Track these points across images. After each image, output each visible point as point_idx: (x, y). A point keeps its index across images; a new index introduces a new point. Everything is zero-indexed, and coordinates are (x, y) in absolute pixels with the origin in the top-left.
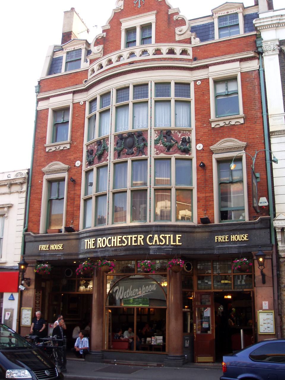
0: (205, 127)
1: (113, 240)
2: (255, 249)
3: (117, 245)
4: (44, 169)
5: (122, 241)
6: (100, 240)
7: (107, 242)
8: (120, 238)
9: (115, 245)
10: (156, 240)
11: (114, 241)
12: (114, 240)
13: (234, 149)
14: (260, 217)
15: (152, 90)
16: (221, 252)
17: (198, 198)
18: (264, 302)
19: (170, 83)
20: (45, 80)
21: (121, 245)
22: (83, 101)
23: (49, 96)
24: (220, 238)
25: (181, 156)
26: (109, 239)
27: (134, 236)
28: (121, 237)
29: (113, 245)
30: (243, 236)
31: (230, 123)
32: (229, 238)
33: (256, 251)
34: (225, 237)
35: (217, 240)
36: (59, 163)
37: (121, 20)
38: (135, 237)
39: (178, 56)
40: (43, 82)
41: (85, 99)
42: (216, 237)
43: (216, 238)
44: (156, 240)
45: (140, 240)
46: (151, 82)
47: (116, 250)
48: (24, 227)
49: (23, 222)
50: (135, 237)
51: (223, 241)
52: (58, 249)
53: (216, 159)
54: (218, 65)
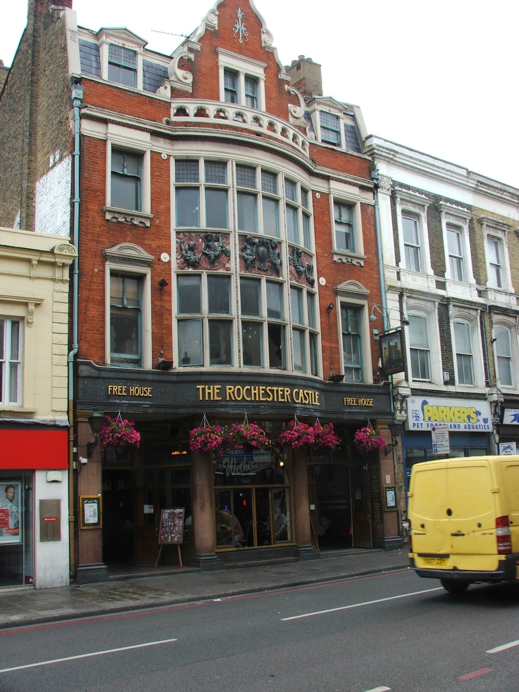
0: (326, 257)
1: (253, 392)
2: (379, 416)
3: (214, 398)
4: (114, 251)
5: (266, 394)
6: (230, 389)
7: (243, 392)
8: (263, 390)
9: (257, 399)
10: (302, 397)
11: (255, 394)
12: (209, 391)
13: (130, 261)
14: (384, 381)
15: (231, 173)
16: (350, 417)
17: (323, 347)
18: (387, 476)
19: (197, 161)
20: (91, 82)
21: (265, 399)
22: (167, 153)
23: (110, 120)
24: (349, 400)
25: (193, 271)
26: (247, 389)
27: (280, 389)
28: (264, 388)
29: (253, 399)
30: (146, 389)
31: (133, 221)
32: (128, 391)
33: (91, 410)
34: (122, 388)
35: (112, 391)
36: (140, 250)
37: (220, 49)
38: (281, 390)
39: (192, 119)
40: (87, 83)
41: (170, 152)
42: (110, 386)
43: (110, 389)
44: (302, 397)
45: (229, 393)
46: (232, 161)
47: (272, 407)
48: (70, 349)
49: (65, 339)
50: (281, 390)
51: (119, 394)
52: (144, 396)
53: (111, 270)
54: (134, 130)
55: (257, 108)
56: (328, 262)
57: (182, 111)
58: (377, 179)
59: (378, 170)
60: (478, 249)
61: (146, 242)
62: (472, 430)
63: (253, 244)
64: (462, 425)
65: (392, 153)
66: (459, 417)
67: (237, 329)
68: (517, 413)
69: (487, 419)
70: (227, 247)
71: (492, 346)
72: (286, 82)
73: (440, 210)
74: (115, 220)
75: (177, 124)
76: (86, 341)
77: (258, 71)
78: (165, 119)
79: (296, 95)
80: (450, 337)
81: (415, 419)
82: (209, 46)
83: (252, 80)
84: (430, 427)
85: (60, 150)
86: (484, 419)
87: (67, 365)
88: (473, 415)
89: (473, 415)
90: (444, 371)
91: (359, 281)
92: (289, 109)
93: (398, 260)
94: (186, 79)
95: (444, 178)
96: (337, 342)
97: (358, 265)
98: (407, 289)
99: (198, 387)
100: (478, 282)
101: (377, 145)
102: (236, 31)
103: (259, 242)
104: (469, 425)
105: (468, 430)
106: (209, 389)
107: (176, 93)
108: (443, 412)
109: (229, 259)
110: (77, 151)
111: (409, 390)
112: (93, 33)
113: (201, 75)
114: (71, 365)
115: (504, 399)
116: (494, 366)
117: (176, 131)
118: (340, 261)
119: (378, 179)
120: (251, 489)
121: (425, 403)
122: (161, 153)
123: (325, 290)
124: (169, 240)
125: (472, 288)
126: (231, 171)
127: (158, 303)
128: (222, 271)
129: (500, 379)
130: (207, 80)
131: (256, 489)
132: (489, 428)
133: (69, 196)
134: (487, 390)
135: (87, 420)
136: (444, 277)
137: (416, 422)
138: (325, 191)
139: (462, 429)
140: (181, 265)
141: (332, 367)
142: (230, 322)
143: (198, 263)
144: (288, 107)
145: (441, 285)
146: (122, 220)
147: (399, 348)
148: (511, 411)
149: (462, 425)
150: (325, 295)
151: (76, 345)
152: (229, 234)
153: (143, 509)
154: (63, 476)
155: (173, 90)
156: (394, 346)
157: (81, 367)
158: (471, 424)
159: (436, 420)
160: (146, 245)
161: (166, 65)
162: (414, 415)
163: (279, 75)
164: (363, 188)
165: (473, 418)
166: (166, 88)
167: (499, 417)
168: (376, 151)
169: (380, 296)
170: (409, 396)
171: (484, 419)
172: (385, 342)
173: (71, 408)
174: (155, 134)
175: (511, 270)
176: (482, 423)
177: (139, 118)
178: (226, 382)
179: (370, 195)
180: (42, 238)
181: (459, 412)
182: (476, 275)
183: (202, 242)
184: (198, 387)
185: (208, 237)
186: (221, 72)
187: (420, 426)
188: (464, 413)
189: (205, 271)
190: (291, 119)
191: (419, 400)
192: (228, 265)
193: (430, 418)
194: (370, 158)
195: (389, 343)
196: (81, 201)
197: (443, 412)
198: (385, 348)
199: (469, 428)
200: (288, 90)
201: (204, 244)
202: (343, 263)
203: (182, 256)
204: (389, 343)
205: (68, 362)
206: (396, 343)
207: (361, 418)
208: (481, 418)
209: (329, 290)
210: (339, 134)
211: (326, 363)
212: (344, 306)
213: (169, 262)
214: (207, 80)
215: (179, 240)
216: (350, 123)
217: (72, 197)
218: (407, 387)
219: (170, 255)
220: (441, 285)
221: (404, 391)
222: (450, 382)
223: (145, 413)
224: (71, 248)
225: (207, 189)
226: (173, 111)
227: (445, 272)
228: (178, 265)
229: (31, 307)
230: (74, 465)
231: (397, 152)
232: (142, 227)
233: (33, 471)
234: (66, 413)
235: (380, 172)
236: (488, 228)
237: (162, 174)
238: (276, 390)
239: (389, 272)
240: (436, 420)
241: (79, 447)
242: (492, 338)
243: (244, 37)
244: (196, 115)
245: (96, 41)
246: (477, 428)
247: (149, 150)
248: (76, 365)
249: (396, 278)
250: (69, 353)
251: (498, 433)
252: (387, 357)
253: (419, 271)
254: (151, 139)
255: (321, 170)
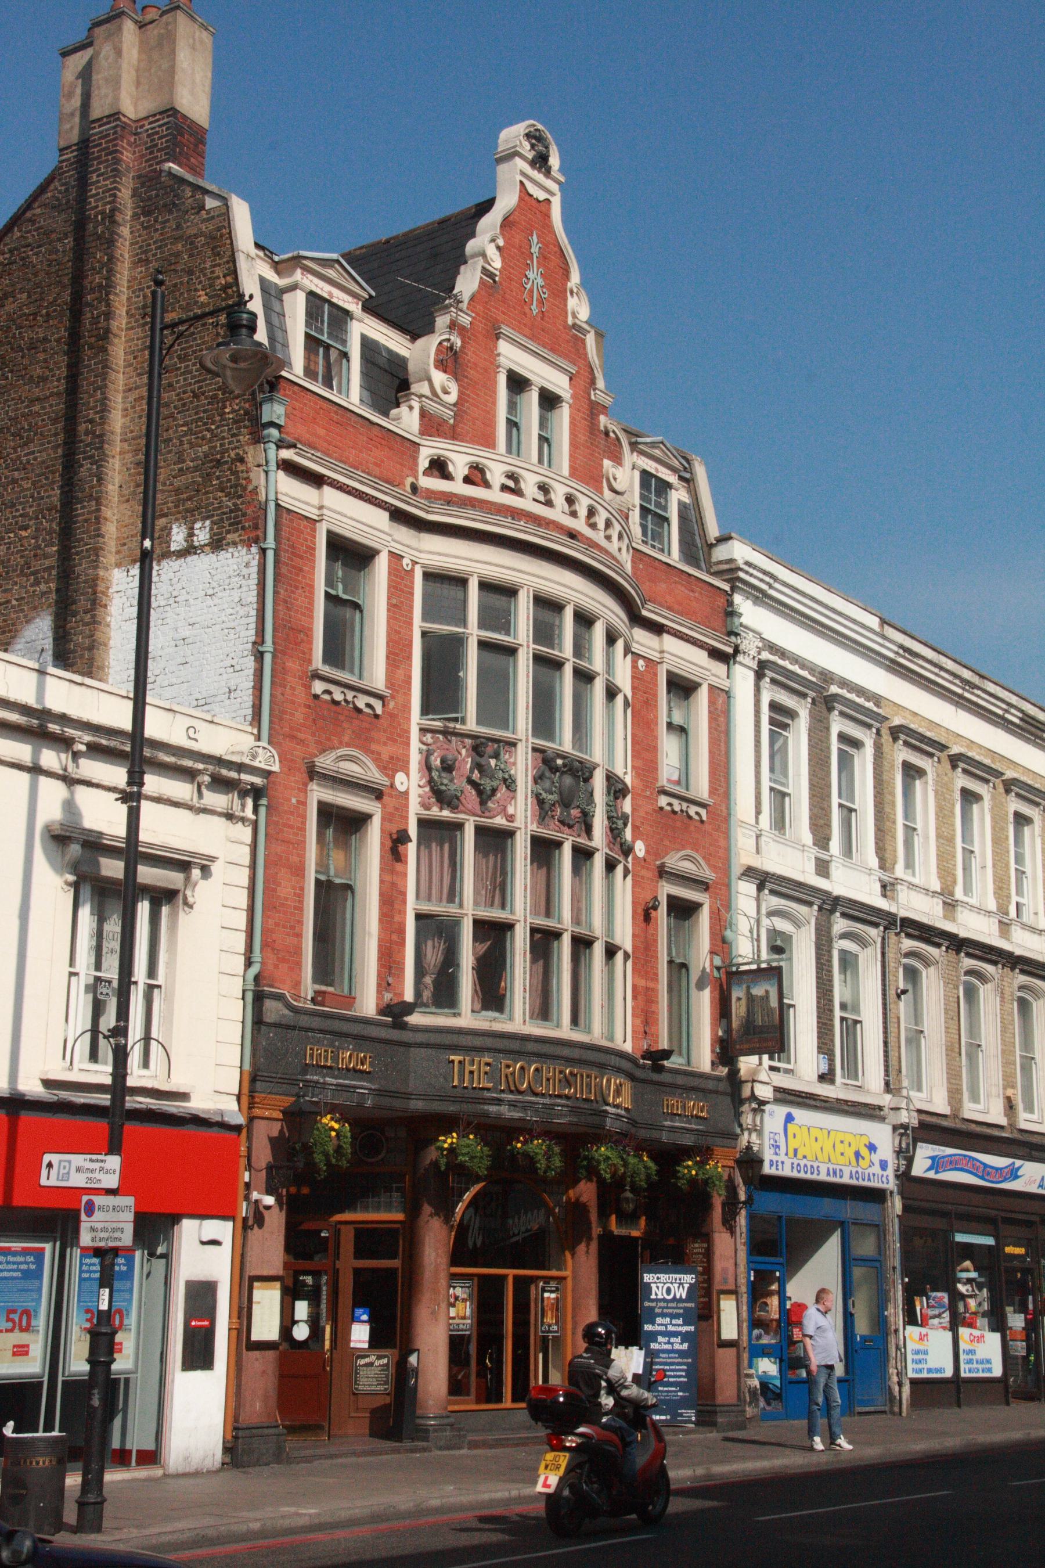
23: (329, 478)
48: (248, 963)
49: (239, 942)
55: (550, 466)
56: (649, 808)
57: (439, 467)
58: (737, 635)
59: (740, 615)
60: (885, 791)
61: (374, 747)
62: (861, 1183)
63: (554, 769)
64: (846, 1171)
65: (767, 579)
66: (842, 1154)
67: (520, 942)
68: (936, 1154)
69: (886, 1162)
70: (512, 772)
71: (897, 1004)
72: (600, 408)
73: (829, 705)
74: (326, 697)
75: (432, 495)
76: (273, 949)
77: (559, 383)
78: (410, 480)
79: (618, 439)
80: (831, 981)
81: (772, 1151)
82: (483, 318)
83: (549, 401)
84: (795, 1170)
85: (213, 523)
86: (881, 1161)
87: (241, 996)
88: (864, 1152)
89: (864, 1152)
90: (819, 1052)
91: (697, 851)
92: (604, 470)
93: (758, 812)
94: (446, 392)
95: (792, 609)
96: (655, 978)
97: (696, 817)
98: (773, 875)
99: (452, 1057)
100: (882, 867)
101: (748, 564)
102: (528, 287)
103: (565, 765)
104: (857, 1172)
105: (854, 1182)
106: (472, 1063)
107: (431, 425)
108: (816, 1140)
109: (514, 798)
110: (270, 542)
111: (771, 1089)
112: (271, 259)
113: (469, 384)
114: (249, 996)
115: (919, 1123)
116: (899, 1047)
117: (433, 513)
118: (668, 808)
119: (739, 634)
120: (504, 1277)
121: (789, 1118)
122: (403, 557)
123: (643, 867)
124: (408, 744)
125: (806, 854)
126: (524, 611)
127: (388, 878)
128: (500, 821)
129: (906, 1076)
130: (478, 395)
131: (515, 1277)
132: (889, 1182)
133: (251, 634)
134: (886, 1100)
135: (281, 1116)
136: (828, 851)
137: (775, 1158)
138: (655, 656)
139: (846, 1180)
140: (427, 800)
141: (647, 1029)
142: (510, 927)
143: (458, 798)
144: (602, 466)
145: (823, 868)
146: (338, 696)
147: (774, 1003)
148: (927, 1149)
149: (846, 1171)
150: (643, 877)
151: (257, 956)
152: (514, 745)
153: (642, 1278)
154: (222, 1229)
155: (424, 414)
156: (762, 998)
157: (269, 1004)
158: (860, 1170)
159: (805, 1157)
160: (373, 752)
161: (403, 352)
162: (772, 1142)
163: (592, 393)
164: (716, 654)
165: (863, 1158)
166: (411, 408)
167: (905, 1159)
168: (741, 574)
169: (728, 886)
170: (768, 1102)
171: (881, 1161)
172: (739, 984)
173: (246, 1091)
174: (398, 516)
175: (937, 840)
176: (877, 1169)
177: (328, 455)
178: (499, 1051)
179: (720, 668)
180: (84, 687)
181: (842, 1142)
182: (881, 850)
183: (467, 756)
184: (452, 1057)
185: (479, 746)
186: (502, 380)
187: (780, 1167)
188: (850, 1145)
189: (472, 818)
190: (607, 494)
191: (781, 1111)
192: (511, 810)
193: (796, 1151)
194: (726, 587)
195: (748, 988)
196: (275, 649)
197: (816, 1140)
198: (739, 999)
199: (857, 1179)
200: (606, 427)
201: (470, 760)
202: (674, 812)
203: (431, 781)
204: (748, 988)
205: (244, 991)
206: (767, 992)
207: (688, 1140)
208: (876, 1158)
209: (648, 869)
210: (546, 445)
211: (638, 1021)
212: (328, 813)
213: (406, 793)
214: (478, 395)
215: (424, 747)
216: (686, 498)
217: (259, 640)
218: (768, 1084)
219: (408, 775)
220: (823, 868)
221: (764, 1092)
222: (826, 1077)
223: (360, 1105)
224: (269, 754)
225: (483, 645)
226: (423, 463)
227: (829, 839)
228: (419, 799)
229: (196, 873)
230: (244, 1209)
231: (775, 579)
232: (368, 715)
233: (175, 1219)
234: (235, 1098)
235: (743, 620)
236: (905, 749)
237: (402, 602)
238: (460, 1062)
239: (744, 835)
240: (805, 1157)
241: (253, 1171)
242: (898, 988)
243: (541, 302)
244: (467, 480)
245: (276, 276)
246: (869, 1180)
247: (387, 549)
248: (259, 998)
249: (754, 850)
250: (245, 971)
251: (901, 1193)
252: (743, 1014)
253: (851, 858)
254: (390, 527)
255: (653, 612)
